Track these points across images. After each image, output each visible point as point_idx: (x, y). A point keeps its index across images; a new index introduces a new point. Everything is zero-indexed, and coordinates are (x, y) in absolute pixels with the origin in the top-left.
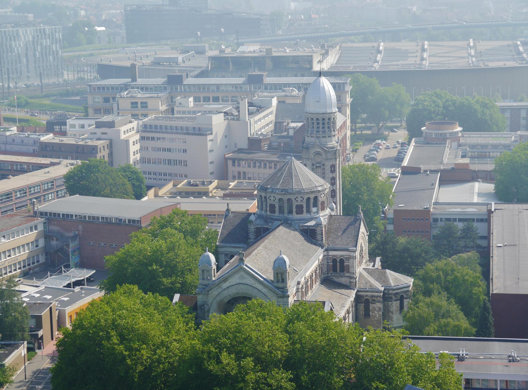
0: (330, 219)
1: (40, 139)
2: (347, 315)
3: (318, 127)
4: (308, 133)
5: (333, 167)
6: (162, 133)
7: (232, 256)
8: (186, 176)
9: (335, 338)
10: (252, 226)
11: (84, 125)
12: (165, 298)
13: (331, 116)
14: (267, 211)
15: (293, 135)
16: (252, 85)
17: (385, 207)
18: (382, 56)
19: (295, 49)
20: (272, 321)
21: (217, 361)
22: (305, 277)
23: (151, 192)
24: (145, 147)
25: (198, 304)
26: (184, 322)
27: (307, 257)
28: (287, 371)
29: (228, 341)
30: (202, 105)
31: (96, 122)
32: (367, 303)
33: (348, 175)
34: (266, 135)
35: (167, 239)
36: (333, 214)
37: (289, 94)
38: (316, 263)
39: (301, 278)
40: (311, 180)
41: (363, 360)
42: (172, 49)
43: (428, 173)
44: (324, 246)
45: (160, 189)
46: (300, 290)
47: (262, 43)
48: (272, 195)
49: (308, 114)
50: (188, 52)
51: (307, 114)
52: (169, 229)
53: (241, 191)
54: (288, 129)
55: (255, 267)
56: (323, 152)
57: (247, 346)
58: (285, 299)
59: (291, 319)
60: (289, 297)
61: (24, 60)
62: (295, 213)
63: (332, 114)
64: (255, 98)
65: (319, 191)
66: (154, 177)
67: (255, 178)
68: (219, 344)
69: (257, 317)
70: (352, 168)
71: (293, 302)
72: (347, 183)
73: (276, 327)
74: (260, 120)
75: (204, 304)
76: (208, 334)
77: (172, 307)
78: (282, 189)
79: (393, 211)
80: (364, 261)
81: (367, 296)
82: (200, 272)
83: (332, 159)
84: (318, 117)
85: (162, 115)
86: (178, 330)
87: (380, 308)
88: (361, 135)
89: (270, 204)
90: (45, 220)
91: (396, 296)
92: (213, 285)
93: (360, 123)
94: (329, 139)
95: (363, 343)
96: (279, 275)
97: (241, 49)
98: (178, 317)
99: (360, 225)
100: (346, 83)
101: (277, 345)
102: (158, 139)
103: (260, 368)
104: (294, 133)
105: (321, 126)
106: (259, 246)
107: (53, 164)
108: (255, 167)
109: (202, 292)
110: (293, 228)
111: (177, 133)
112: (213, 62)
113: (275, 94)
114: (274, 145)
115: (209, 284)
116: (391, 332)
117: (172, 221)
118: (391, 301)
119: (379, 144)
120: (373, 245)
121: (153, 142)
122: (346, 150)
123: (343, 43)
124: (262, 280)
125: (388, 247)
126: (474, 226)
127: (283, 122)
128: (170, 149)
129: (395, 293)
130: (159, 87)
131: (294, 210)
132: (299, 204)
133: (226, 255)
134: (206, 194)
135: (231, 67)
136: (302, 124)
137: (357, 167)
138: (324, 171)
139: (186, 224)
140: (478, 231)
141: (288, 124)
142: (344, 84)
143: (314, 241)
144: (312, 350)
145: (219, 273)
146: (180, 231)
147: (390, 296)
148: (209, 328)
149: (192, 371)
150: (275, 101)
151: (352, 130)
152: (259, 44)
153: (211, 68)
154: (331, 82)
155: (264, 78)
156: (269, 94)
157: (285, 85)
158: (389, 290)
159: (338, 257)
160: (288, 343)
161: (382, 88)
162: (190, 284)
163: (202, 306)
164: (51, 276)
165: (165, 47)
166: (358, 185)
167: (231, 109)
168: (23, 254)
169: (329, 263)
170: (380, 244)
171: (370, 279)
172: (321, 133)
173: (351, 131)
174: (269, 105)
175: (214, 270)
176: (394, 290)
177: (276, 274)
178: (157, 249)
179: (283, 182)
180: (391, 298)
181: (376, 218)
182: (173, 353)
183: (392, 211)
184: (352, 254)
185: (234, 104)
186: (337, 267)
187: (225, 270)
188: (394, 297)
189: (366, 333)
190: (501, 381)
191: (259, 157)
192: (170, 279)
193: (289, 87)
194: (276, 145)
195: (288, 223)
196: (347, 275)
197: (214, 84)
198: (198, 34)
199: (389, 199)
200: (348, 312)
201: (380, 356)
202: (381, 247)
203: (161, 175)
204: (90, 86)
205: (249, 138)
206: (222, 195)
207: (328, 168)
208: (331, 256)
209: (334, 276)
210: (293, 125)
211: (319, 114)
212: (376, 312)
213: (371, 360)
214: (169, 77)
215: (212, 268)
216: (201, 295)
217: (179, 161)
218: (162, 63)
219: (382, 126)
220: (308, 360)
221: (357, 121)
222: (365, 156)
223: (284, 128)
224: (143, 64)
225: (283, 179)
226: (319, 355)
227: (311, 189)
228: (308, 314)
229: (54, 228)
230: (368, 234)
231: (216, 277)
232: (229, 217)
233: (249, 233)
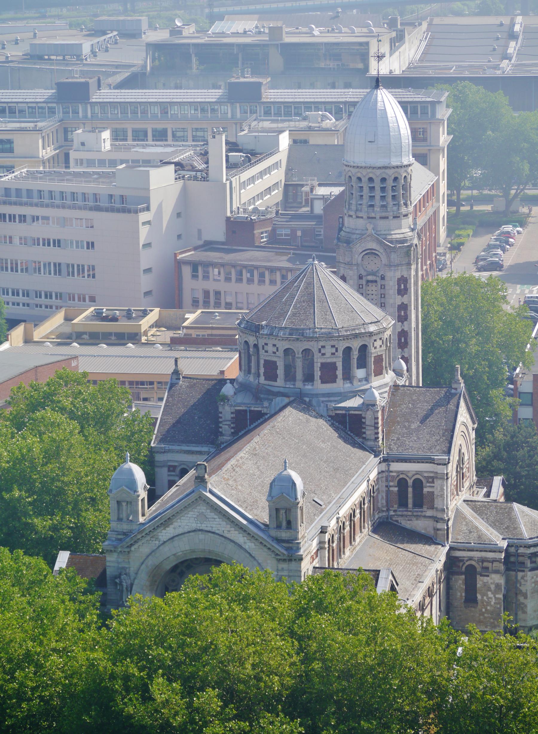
0: (393, 394)
2: (428, 600)
3: (370, 196)
4: (349, 209)
5: (403, 282)
6: (42, 206)
7: (184, 472)
8: (93, 299)
9: (396, 650)
10: (227, 408)
12: (41, 563)
13: (400, 174)
14: (259, 376)
15: (322, 212)
16: (238, 105)
17: (515, 369)
18: (519, 45)
19: (333, 29)
20: (263, 612)
21: (143, 696)
22: (338, 519)
23: (17, 333)
25: (108, 572)
26: (78, 611)
28: (292, 720)
29: (168, 655)
30: (128, 148)
33: (436, 299)
34: (263, 213)
35: (44, 433)
36: (401, 382)
37: (317, 125)
38: (364, 487)
39: (329, 519)
40: (353, 310)
41: (455, 697)
42: (71, 26)
44: (380, 452)
45: (36, 325)
46: (327, 546)
47: (263, 14)
48: (271, 342)
49: (351, 169)
50: (104, 33)
51: (347, 169)
52: (48, 414)
53: (209, 332)
54: (312, 200)
55: (231, 496)
56: (382, 251)
57: (207, 664)
58: (293, 565)
59: (304, 609)
60: (301, 559)
63: (403, 170)
64: (242, 133)
65: (371, 333)
66: (26, 300)
67: (239, 305)
68: (148, 660)
69: (229, 604)
70: (445, 285)
71: (310, 573)
72: (433, 317)
73: (272, 625)
74: (252, 180)
75: (120, 574)
76: (124, 638)
77: (51, 579)
78: (292, 329)
79: (531, 378)
80: (467, 484)
81: (471, 559)
82: (114, 505)
83: (401, 265)
84: (371, 175)
85: (44, 167)
86: (62, 629)
87: (498, 586)
88: (471, 214)
89: (265, 361)
91: (534, 559)
92: (140, 532)
93: (469, 188)
94: (396, 221)
95: (455, 661)
96: (282, 512)
97: (218, 27)
98: (63, 602)
99: (458, 407)
100: (439, 102)
101: (272, 662)
102: (35, 219)
103: (235, 712)
104: (325, 209)
105: (378, 193)
106: (240, 450)
108: (239, 280)
109: (115, 547)
110: (314, 413)
111: (74, 207)
112: (156, 55)
113: (286, 124)
114: (282, 235)
115: (131, 531)
116: (517, 638)
117: (54, 394)
118: (523, 571)
119: (508, 233)
120: (487, 450)
121: (23, 225)
122: (436, 244)
123: (438, 15)
124: (245, 522)
125: (520, 453)
127: (302, 186)
128: (59, 241)
129: (532, 554)
130: (39, 108)
131: (318, 374)
132: (329, 360)
133: (171, 468)
135: (194, 66)
136: (342, 189)
137: (456, 284)
138: (383, 291)
139: (84, 401)
141: (312, 190)
143: (359, 440)
144: (346, 675)
145: (153, 508)
146: (72, 416)
147: (521, 559)
148: (126, 626)
149: (91, 717)
150: (284, 141)
151: (450, 203)
152: (256, 16)
153: (152, 68)
154: (400, 100)
155: (263, 91)
156: (274, 125)
157: (309, 106)
158: (517, 547)
159: (410, 475)
160: (295, 658)
161: (516, 115)
162: (93, 530)
163: (116, 577)
165: (57, 22)
166: (457, 322)
167: (190, 158)
169: (391, 489)
170: (502, 447)
171: (477, 524)
172: (377, 209)
173: (448, 206)
174: (273, 149)
176: (529, 547)
177: (275, 512)
178: (22, 455)
179: (294, 314)
180: (524, 563)
181: (493, 393)
182: (51, 679)
183: (530, 378)
184: (440, 469)
185: (197, 146)
187: (167, 501)
188: (529, 561)
189: (464, 639)
191: (250, 260)
192: (50, 519)
194: (286, 235)
195: (304, 402)
196: (429, 513)
197: (156, 102)
199: (523, 352)
200: (430, 593)
201: (491, 688)
202: (505, 454)
203: (40, 297)
205: (228, 219)
206: (168, 341)
207: (392, 286)
208: (394, 474)
209: (402, 516)
210: (322, 191)
211: (374, 168)
212: (490, 594)
213: (473, 696)
214: (60, 86)
215: (138, 496)
216: (115, 555)
217: (78, 266)
218: (46, 57)
219: (516, 195)
220: (338, 696)
221: (462, 184)
222: (478, 259)
223: (304, 198)
224: (7, 57)
225: (294, 308)
226: (362, 684)
227: (354, 330)
228: (341, 598)
230: (476, 426)
231: (147, 515)
232: (178, 387)
233: (221, 422)
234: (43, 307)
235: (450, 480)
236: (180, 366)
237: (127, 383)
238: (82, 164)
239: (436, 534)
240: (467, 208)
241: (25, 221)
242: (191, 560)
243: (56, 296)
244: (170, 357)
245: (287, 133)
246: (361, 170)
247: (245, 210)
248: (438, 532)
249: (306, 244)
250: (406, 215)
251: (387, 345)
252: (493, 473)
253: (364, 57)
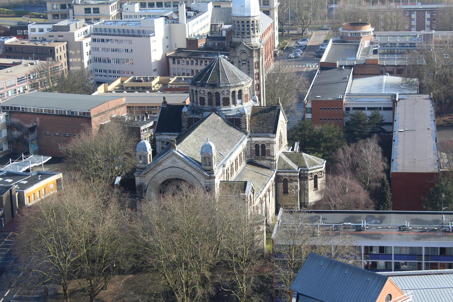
1: (4, 42)
8: (132, 73)
11: (43, 29)
14: (198, 103)
15: (225, 35)
24: (96, 48)
27: (232, 143)
31: (53, 26)
32: (286, 182)
43: (343, 67)
44: (247, 133)
49: (235, 18)
53: (180, 86)
56: (248, 51)
58: (212, 180)
62: (222, 105)
63: (251, 18)
66: (105, 74)
81: (285, 176)
84: (243, 20)
89: (200, 97)
90: (6, 113)
102: (107, 40)
104: (226, 34)
107: (15, 64)
108: (192, 64)
114: (209, 45)
118: (307, 180)
126: (380, 114)
127: (217, 25)
132: (226, 97)
134: (149, 88)
140: (383, 118)
151: (280, 30)
159: (260, 142)
163: (140, 187)
164: (12, 162)
167: (171, 14)
169: (252, 148)
172: (246, 34)
175: (150, 155)
177: (204, 159)
179: (211, 78)
184: (272, 140)
186: (259, 152)
190: (395, 247)
196: (268, 158)
205: (187, 39)
208: (254, 142)
209: (257, 159)
211: (244, 17)
212: (293, 190)
215: (148, 153)
229: (15, 120)
230: (287, 122)
234: (112, 77)
235: (276, 144)
236: (166, 100)
237: (146, 107)
239: (271, 166)
240: (287, 32)
241: (104, 42)
242: (170, 179)
243: (117, 72)
244: (120, 106)
246: (239, 18)
247: (194, 35)
248: (272, 165)
249: (220, 49)
250: (257, 36)
251: (250, 90)
252: (296, 140)
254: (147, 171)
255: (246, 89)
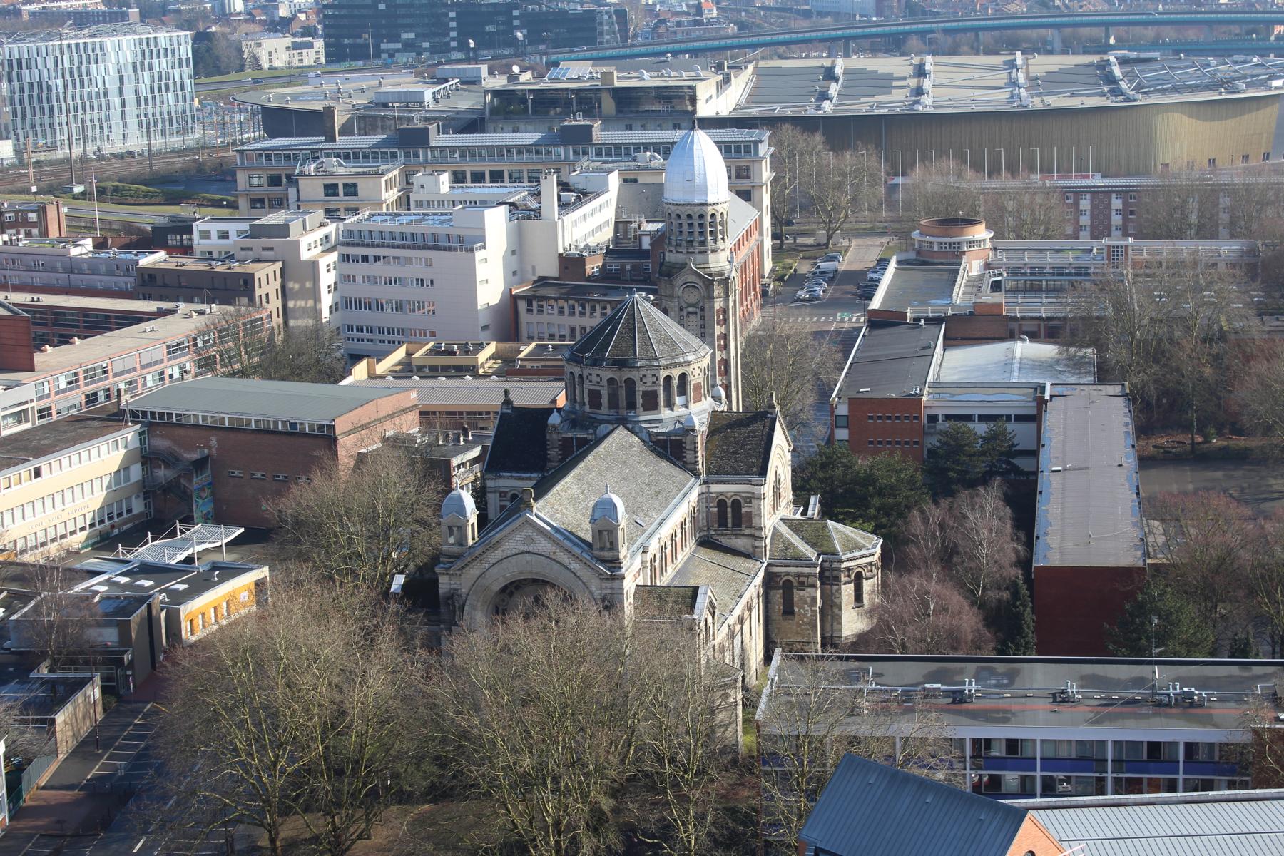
1: (137, 263)
8: (433, 334)
11: (227, 232)
14: (584, 404)
27: (663, 499)
32: (788, 588)
43: (922, 322)
44: (700, 475)
50: (446, 81)
53: (543, 363)
58: (616, 584)
61: (115, 101)
66: (369, 336)
75: (453, 595)
81: (788, 574)
84: (689, 212)
89: (590, 391)
102: (376, 259)
104: (651, 244)
107: (162, 313)
108: (572, 313)
126: (1008, 431)
127: (631, 222)
132: (650, 389)
134: (472, 370)
142: (756, 143)
151: (774, 236)
157: (639, 147)
159: (729, 496)
163: (448, 598)
164: (153, 539)
167: (524, 198)
168: (95, 500)
171: (793, 541)
175: (473, 525)
177: (599, 533)
179: (616, 346)
190: (1043, 741)
193: (646, 150)
196: (747, 532)
198: (469, 43)
204: (241, 152)
205: (560, 255)
211: (692, 205)
229: (161, 443)
238: (421, 205)
240: (791, 241)
241: (367, 261)
242: (520, 581)
245: (616, 172)
252: (813, 491)
253: (693, 100)
254: (466, 562)
255: (697, 372)
